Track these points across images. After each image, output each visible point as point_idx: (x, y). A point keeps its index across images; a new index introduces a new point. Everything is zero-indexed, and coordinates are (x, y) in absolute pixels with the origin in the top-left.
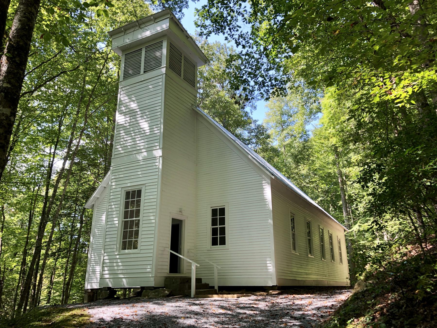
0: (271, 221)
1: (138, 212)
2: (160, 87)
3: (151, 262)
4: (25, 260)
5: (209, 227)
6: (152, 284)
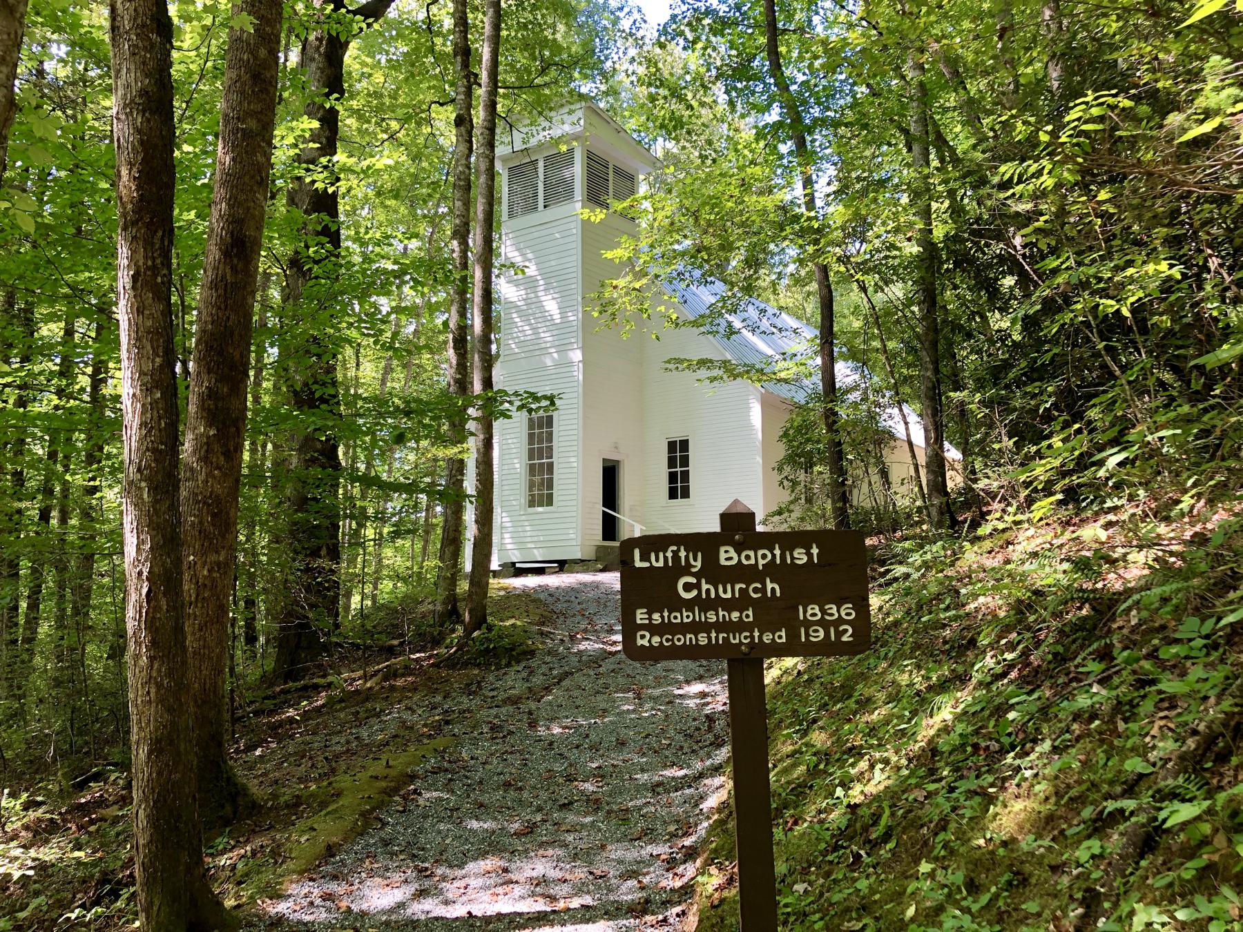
0: (759, 460)
1: (550, 449)
2: (574, 238)
3: (574, 525)
5: (663, 471)
6: (579, 556)
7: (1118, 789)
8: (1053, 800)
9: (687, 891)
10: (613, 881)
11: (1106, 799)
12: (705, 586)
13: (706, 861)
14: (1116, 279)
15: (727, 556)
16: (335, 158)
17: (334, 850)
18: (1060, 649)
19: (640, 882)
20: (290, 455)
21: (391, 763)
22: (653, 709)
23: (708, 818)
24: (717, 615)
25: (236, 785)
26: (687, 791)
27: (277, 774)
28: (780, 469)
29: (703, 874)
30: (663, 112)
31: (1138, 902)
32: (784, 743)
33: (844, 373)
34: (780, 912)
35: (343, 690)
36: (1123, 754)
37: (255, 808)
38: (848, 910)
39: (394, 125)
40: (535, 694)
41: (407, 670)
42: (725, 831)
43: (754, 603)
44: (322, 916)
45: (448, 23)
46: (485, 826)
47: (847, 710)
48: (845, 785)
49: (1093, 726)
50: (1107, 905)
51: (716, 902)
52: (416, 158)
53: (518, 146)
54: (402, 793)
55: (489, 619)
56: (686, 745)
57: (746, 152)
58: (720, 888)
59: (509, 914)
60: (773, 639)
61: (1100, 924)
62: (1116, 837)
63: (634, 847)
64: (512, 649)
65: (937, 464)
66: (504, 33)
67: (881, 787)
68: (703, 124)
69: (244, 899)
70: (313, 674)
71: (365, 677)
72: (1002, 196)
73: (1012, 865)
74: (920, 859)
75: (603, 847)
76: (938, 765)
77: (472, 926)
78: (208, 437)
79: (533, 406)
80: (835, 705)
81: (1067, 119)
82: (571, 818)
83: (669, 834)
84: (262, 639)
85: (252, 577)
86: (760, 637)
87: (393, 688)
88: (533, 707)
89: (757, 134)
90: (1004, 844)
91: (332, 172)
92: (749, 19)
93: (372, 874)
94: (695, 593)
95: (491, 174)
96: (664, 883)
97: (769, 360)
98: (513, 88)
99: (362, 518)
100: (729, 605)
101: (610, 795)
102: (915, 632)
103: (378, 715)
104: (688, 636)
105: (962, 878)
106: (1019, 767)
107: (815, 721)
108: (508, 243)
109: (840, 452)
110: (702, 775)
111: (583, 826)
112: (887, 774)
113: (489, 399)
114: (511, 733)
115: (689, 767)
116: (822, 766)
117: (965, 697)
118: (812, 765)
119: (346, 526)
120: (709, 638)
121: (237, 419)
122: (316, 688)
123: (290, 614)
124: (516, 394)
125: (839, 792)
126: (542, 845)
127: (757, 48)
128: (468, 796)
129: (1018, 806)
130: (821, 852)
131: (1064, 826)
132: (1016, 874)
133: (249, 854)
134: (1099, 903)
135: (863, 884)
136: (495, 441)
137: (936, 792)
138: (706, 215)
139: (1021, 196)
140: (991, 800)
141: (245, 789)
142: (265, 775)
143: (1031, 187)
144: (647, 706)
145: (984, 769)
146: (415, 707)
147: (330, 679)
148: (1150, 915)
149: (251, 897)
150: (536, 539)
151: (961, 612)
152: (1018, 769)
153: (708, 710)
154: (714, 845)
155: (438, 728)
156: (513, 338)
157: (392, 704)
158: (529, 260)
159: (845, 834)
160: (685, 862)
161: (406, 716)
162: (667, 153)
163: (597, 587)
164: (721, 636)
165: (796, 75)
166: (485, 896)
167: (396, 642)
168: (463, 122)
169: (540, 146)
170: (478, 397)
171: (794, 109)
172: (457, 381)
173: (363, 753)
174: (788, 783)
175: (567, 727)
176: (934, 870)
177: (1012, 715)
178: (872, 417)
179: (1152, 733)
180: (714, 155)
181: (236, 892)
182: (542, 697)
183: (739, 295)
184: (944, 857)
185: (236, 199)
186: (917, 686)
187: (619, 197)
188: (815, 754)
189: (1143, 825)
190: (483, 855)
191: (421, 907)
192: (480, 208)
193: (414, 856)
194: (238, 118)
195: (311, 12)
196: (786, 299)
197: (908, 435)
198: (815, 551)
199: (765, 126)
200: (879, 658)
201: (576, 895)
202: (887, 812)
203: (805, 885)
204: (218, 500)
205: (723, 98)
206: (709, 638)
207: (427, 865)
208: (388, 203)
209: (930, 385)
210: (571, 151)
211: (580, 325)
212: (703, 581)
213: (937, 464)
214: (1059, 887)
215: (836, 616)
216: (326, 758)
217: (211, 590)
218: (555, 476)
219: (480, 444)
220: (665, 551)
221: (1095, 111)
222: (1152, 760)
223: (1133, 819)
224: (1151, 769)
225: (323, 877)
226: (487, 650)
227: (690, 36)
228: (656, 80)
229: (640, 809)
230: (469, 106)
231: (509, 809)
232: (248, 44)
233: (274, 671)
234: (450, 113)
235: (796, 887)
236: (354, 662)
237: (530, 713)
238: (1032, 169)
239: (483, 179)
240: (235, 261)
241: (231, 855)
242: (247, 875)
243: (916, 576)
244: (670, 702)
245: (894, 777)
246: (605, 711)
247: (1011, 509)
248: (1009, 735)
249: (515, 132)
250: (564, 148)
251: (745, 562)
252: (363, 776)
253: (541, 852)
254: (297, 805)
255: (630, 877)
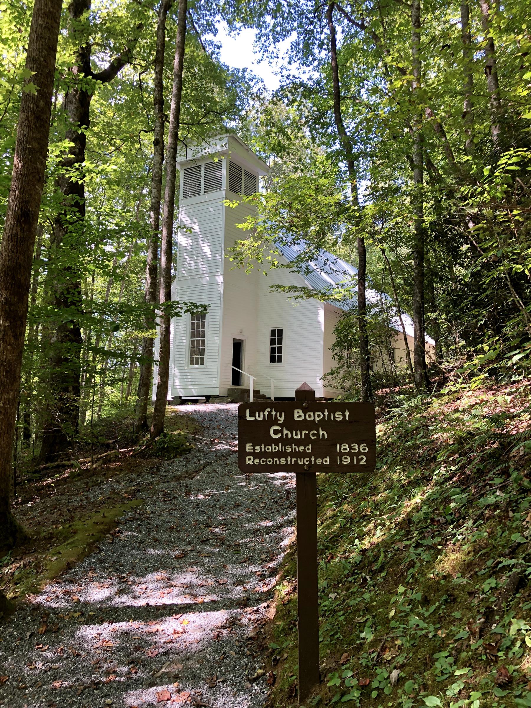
1: (204, 332)
4: (364, 298)
5: (268, 347)
6: (218, 394)
7: (507, 551)
8: (472, 554)
9: (270, 594)
10: (230, 587)
11: (500, 557)
12: (285, 432)
13: (282, 576)
14: (523, 254)
15: (298, 415)
16: (83, 164)
17: (71, 565)
18: (482, 467)
19: (244, 587)
20: (53, 333)
21: (105, 515)
22: (256, 485)
23: (284, 551)
24: (291, 448)
25: (15, 526)
26: (273, 535)
27: (40, 518)
28: (333, 349)
29: (279, 585)
30: (274, 141)
31: (513, 618)
32: (328, 510)
33: (371, 295)
34: (320, 609)
35: (80, 469)
36: (512, 531)
37: (26, 540)
38: (358, 610)
39: (119, 142)
40: (190, 475)
41: (117, 458)
42: (293, 560)
43: (312, 442)
44: (63, 604)
45: (151, 84)
46: (159, 552)
47: (364, 493)
48: (360, 537)
49: (496, 513)
50: (497, 618)
51: (286, 602)
52: (131, 162)
53: (190, 157)
54: (111, 532)
55: (165, 430)
56: (274, 507)
57: (320, 166)
58: (288, 594)
59: (170, 605)
60: (322, 462)
61: (493, 628)
62: (504, 578)
63: (242, 567)
64: (178, 448)
65: (421, 351)
66: (184, 92)
67: (380, 540)
68: (297, 149)
69: (18, 594)
70: (63, 458)
71: (93, 462)
72: (461, 204)
73: (448, 590)
74: (399, 583)
75: (225, 566)
76: (412, 529)
77: (149, 611)
78: (5, 327)
79: (195, 311)
80: (357, 489)
81: (499, 163)
82: (207, 548)
83: (261, 559)
84: (34, 436)
85: (28, 403)
86: (315, 461)
87: (108, 469)
88: (188, 483)
89: (327, 156)
90: (445, 577)
91: (81, 172)
92: (324, 90)
93: (92, 580)
94: (279, 435)
95: (174, 172)
96: (257, 589)
97: (330, 287)
98: (188, 124)
99: (92, 371)
100: (298, 443)
101: (230, 536)
102: (403, 449)
103: (99, 485)
104: (275, 459)
105: (420, 596)
106: (455, 534)
107: (346, 498)
108: (183, 212)
109: (367, 341)
110: (281, 526)
111: (214, 554)
112: (383, 532)
113: (169, 306)
114: (175, 498)
115: (275, 520)
116: (348, 526)
117: (429, 490)
118: (343, 525)
119: (84, 376)
120: (287, 461)
121: (22, 317)
122: (64, 467)
123: (50, 425)
124: (185, 303)
125: (357, 542)
126: (191, 564)
127: (329, 107)
128: (149, 535)
129: (453, 556)
130: (345, 575)
131: (477, 570)
132: (450, 596)
133: (22, 566)
134: (493, 616)
135: (367, 596)
136: (172, 329)
137: (410, 545)
138: (297, 205)
139: (472, 205)
140: (439, 552)
141: (21, 529)
142: (33, 518)
143: (478, 200)
144: (253, 484)
145: (436, 533)
146: (121, 481)
147: (72, 462)
148: (519, 625)
149: (22, 592)
150: (193, 383)
151: (429, 440)
152: (455, 535)
153: (287, 487)
154: (286, 568)
155: (133, 494)
156: (184, 268)
157: (107, 478)
158: (195, 223)
159: (359, 566)
160: (270, 577)
161: (116, 486)
162: (276, 164)
163: (228, 412)
164: (293, 460)
165: (350, 125)
166: (157, 594)
167: (111, 442)
168: (158, 143)
169: (203, 158)
170: (162, 305)
171: (348, 144)
172: (150, 293)
173: (90, 508)
174: (329, 534)
175: (207, 495)
176: (405, 591)
177: (452, 505)
178: (387, 320)
179: (527, 519)
180: (302, 167)
181: (14, 589)
182: (194, 477)
183: (313, 251)
184: (412, 583)
185: (24, 189)
186: (403, 482)
187: (248, 194)
188: (345, 518)
189: (519, 573)
190: (156, 569)
191: (120, 600)
192: (166, 193)
193: (117, 569)
194: (27, 142)
195: (71, 77)
196: (341, 249)
197: (404, 331)
198: (347, 414)
199: (332, 152)
200: (383, 463)
201: (208, 594)
202: (382, 555)
203: (336, 594)
204: (9, 363)
205: (308, 134)
206: (287, 461)
207: (124, 575)
208: (114, 187)
209: (418, 305)
210: (220, 161)
211: (223, 262)
212: (285, 429)
213: (421, 351)
214: (472, 605)
215: (357, 450)
216: (68, 510)
217: (4, 415)
218: (206, 348)
219: (163, 330)
220: (264, 411)
221: (514, 160)
222: (526, 535)
223: (514, 570)
224: (525, 541)
225: (64, 581)
226: (163, 448)
227: (291, 98)
228: (270, 122)
229: (246, 544)
230: (162, 134)
231: (172, 543)
232: (33, 98)
233: (40, 456)
234: (151, 137)
235: (330, 595)
236: (87, 452)
237: (187, 486)
238: (479, 189)
239: (169, 177)
240: (23, 225)
241: (11, 567)
242: (20, 579)
243: (405, 414)
244: (266, 482)
245: (387, 534)
246: (229, 486)
247: (460, 380)
248: (451, 514)
249: (188, 149)
250: (216, 160)
251: (308, 419)
252: (90, 522)
253: (189, 569)
254: (51, 538)
255: (239, 584)
